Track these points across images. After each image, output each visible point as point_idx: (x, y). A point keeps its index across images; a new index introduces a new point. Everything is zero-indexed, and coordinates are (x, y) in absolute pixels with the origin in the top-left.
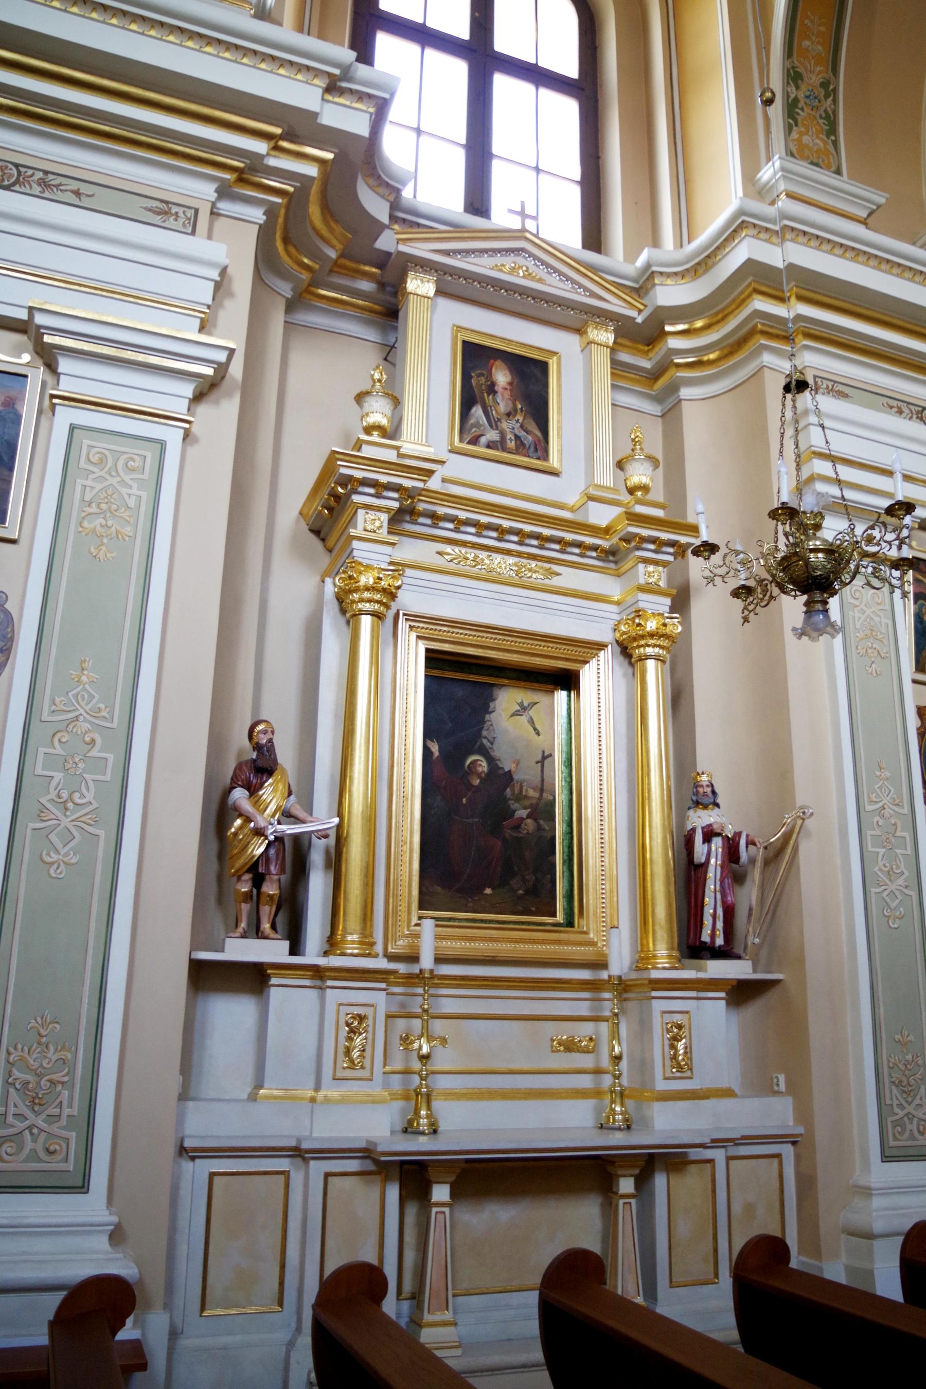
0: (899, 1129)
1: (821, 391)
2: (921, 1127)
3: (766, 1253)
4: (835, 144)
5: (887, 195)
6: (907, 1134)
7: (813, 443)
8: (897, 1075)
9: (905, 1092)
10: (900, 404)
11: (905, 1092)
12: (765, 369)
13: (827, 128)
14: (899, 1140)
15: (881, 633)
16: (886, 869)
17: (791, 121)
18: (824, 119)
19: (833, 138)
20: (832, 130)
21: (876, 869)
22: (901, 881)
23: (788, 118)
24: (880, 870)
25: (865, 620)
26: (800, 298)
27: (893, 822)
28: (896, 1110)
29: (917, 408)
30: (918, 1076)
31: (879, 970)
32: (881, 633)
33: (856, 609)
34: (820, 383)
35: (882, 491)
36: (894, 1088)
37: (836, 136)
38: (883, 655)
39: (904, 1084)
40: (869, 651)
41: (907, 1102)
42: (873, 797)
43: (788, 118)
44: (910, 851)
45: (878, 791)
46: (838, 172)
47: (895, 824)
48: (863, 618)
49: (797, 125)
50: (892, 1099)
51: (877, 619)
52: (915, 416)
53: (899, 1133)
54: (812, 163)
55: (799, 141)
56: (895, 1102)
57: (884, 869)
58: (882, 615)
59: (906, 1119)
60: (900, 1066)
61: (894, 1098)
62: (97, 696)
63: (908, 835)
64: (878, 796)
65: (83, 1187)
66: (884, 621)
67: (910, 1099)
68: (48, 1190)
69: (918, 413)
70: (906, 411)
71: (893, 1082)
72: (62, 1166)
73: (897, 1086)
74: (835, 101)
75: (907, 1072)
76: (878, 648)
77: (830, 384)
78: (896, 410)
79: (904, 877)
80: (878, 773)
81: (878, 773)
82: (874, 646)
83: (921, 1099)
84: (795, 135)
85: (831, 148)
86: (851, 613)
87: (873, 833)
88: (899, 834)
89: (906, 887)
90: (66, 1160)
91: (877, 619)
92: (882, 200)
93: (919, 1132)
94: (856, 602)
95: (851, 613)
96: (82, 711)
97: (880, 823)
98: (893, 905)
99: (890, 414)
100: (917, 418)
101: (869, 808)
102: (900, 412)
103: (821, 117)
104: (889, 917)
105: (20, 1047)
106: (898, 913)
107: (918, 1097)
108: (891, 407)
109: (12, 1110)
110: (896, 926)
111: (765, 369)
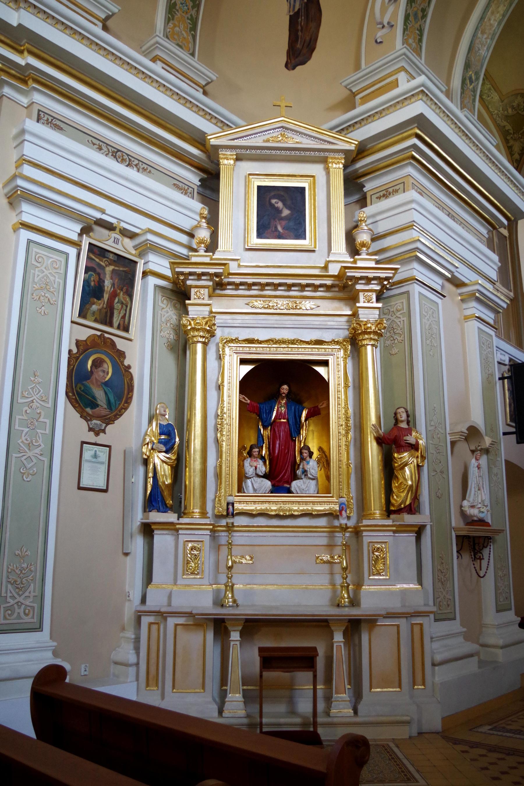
0: (10, 612)
1: (42, 121)
2: (27, 611)
3: (50, 677)
4: (194, 37)
5: (120, 8)
6: (15, 615)
7: (25, 153)
8: (13, 577)
9: (18, 588)
10: (101, 143)
11: (18, 588)
12: (4, 97)
13: (191, 26)
14: (8, 620)
15: (53, 288)
16: (28, 442)
17: (170, 16)
18: (190, 20)
19: (193, 32)
20: (194, 28)
21: (19, 441)
22: (37, 451)
23: (169, 13)
24: (22, 442)
25: (43, 277)
26: (30, 53)
27: (38, 412)
28: (9, 600)
29: (113, 149)
30: (30, 577)
31: (10, 508)
32: (53, 288)
33: (37, 269)
34: (42, 116)
35: (83, 201)
36: (9, 586)
37: (195, 32)
38: (52, 302)
39: (17, 583)
40: (42, 298)
41: (18, 594)
42: (26, 394)
43: (169, 13)
44: (48, 431)
45: (30, 390)
46: (193, 54)
47: (40, 413)
48: (41, 275)
49: (173, 19)
50: (6, 592)
51: (52, 278)
52: (110, 154)
53: (9, 615)
54: (178, 45)
55: (173, 29)
56: (9, 594)
57: (25, 441)
58: (57, 276)
59: (16, 606)
60: (17, 571)
61: (9, 591)
62: (42, 391)
63: (48, 422)
64: (29, 393)
65: (39, 628)
66: (57, 280)
67: (21, 593)
68: (25, 631)
69: (113, 152)
70: (105, 149)
71: (10, 582)
72: (32, 620)
73: (12, 584)
74: (198, 12)
75: (21, 575)
76: (49, 297)
77: (50, 119)
78: (97, 146)
79: (40, 448)
80: (33, 379)
81: (33, 379)
82: (46, 295)
83: (30, 593)
84: (171, 25)
85: (190, 38)
86: (32, 271)
87: (21, 417)
88: (41, 419)
89: (41, 455)
90: (33, 617)
91: (52, 278)
92: (116, 10)
93: (25, 614)
94: (38, 265)
95: (32, 271)
96: (35, 397)
97: (28, 412)
98: (29, 466)
99: (93, 149)
100: (112, 155)
101: (20, 401)
102: (100, 149)
103: (188, 18)
104: (24, 473)
105: (12, 564)
106: (31, 471)
107: (28, 591)
108: (94, 144)
109: (9, 594)
110: (28, 479)
111: (4, 97)
